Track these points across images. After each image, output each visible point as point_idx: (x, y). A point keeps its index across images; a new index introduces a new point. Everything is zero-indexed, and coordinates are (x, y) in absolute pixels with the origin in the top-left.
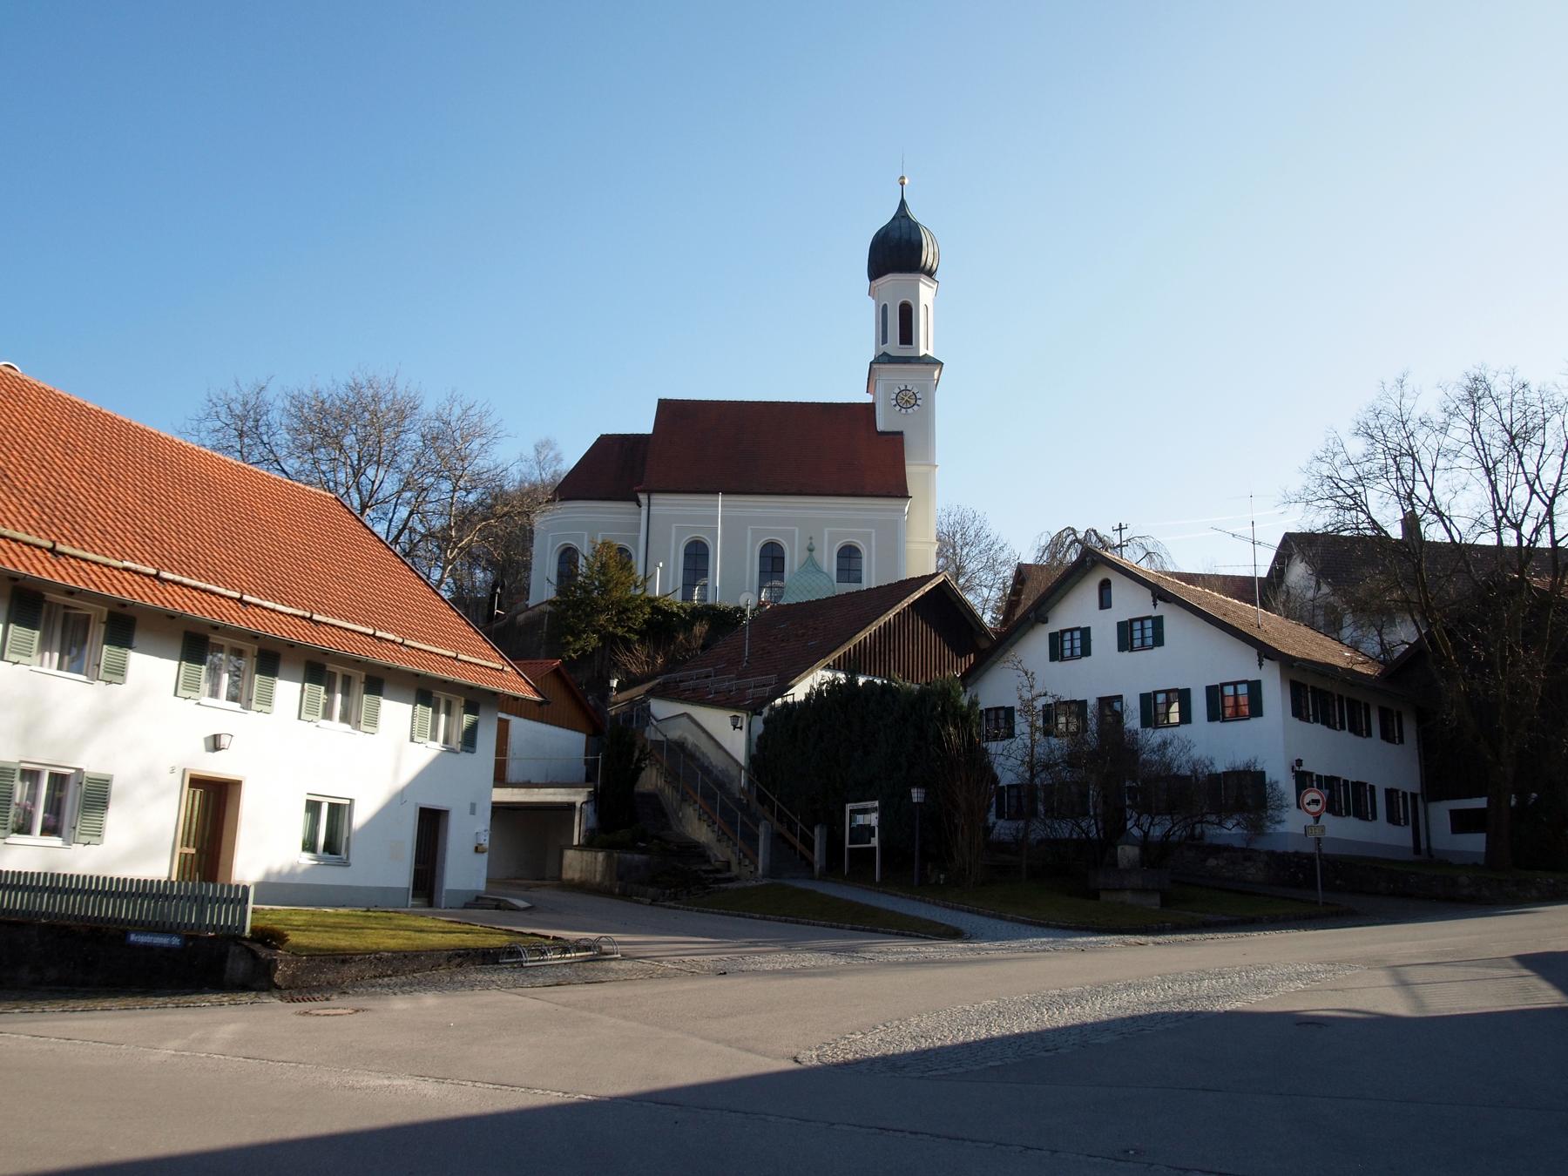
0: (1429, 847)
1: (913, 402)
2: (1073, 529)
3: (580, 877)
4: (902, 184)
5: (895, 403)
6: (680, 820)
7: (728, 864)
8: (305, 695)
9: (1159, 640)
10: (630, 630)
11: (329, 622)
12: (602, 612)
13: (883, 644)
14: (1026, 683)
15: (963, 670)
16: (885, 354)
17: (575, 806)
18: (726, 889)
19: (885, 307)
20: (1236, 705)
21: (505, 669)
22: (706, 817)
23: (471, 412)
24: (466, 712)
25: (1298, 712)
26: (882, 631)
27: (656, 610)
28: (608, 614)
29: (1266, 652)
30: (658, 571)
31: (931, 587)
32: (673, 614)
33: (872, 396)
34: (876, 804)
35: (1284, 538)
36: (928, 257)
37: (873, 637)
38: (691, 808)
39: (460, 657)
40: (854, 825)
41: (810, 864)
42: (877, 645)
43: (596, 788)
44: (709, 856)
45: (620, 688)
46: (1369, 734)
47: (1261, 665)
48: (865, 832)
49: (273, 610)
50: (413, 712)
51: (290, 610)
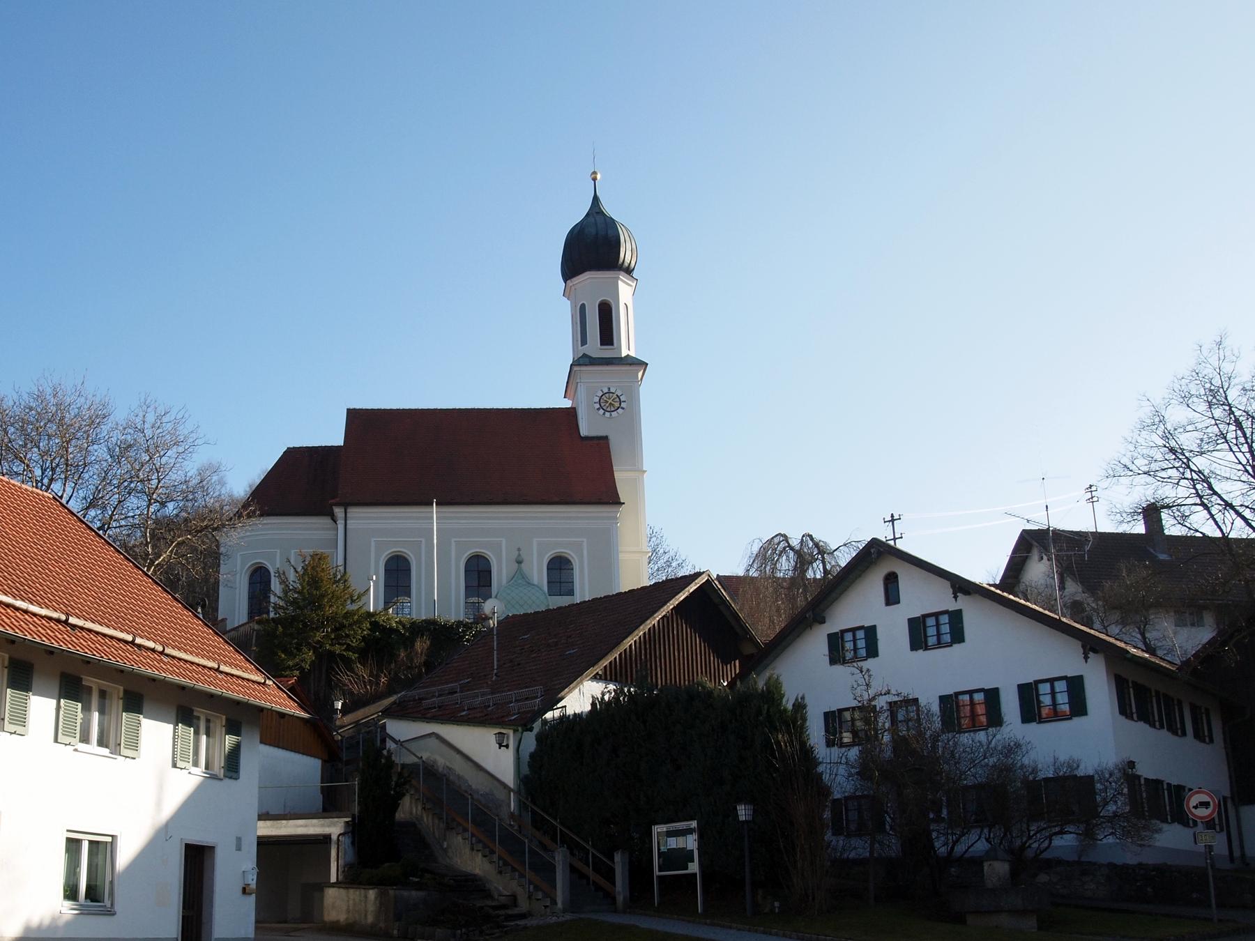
0: (1243, 855)
1: (617, 405)
2: (785, 536)
3: (347, 919)
4: (594, 179)
5: (599, 406)
6: (445, 851)
7: (514, 897)
8: (61, 712)
9: (958, 636)
10: (349, 648)
11: (86, 626)
12: (317, 629)
13: (648, 651)
14: (861, 681)
15: (729, 680)
16: (585, 355)
17: (330, 838)
18: (525, 928)
19: (583, 307)
20: (974, 715)
21: (267, 682)
22: (480, 846)
23: (165, 419)
24: (228, 733)
25: (1124, 710)
26: (647, 636)
27: (375, 626)
28: (323, 632)
29: (1091, 646)
30: (372, 584)
31: (696, 587)
32: (392, 630)
33: (571, 402)
34: (694, 824)
35: (1021, 534)
36: (626, 254)
37: (638, 644)
38: (460, 838)
39: (223, 668)
40: (663, 849)
41: (610, 897)
42: (643, 652)
43: (353, 817)
44: (489, 890)
45: (345, 710)
46: (1184, 734)
47: (1086, 658)
48: (683, 857)
49: (26, 612)
50: (174, 732)
51: (44, 612)
